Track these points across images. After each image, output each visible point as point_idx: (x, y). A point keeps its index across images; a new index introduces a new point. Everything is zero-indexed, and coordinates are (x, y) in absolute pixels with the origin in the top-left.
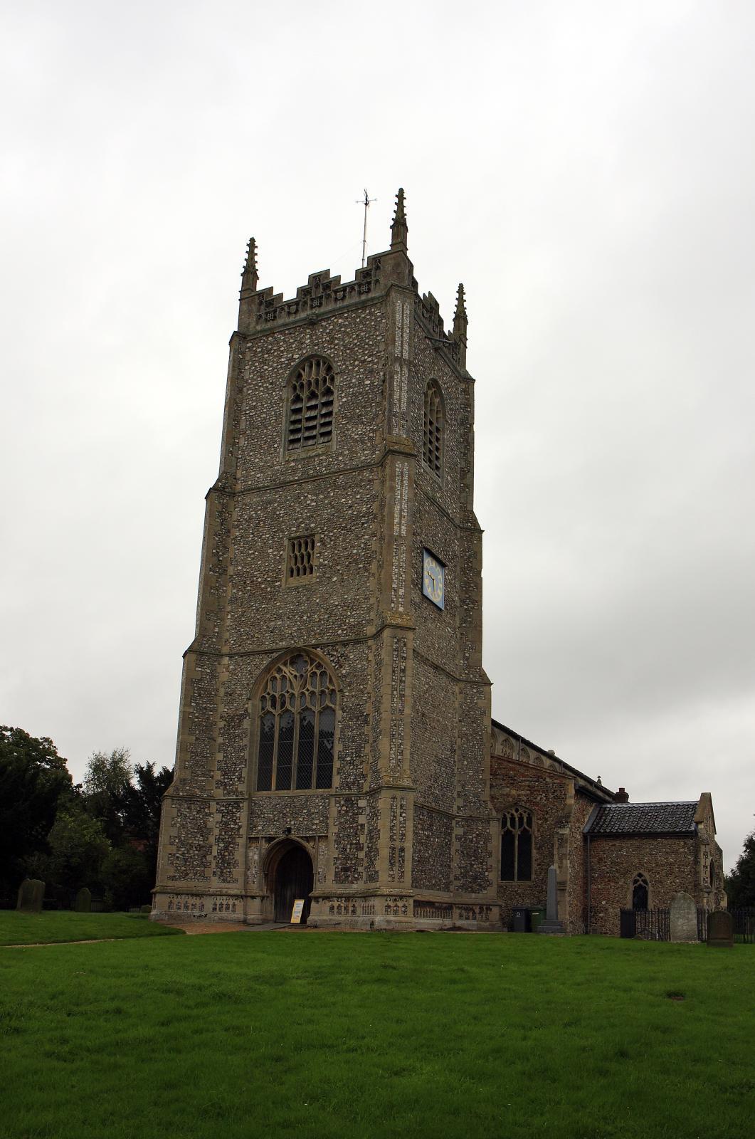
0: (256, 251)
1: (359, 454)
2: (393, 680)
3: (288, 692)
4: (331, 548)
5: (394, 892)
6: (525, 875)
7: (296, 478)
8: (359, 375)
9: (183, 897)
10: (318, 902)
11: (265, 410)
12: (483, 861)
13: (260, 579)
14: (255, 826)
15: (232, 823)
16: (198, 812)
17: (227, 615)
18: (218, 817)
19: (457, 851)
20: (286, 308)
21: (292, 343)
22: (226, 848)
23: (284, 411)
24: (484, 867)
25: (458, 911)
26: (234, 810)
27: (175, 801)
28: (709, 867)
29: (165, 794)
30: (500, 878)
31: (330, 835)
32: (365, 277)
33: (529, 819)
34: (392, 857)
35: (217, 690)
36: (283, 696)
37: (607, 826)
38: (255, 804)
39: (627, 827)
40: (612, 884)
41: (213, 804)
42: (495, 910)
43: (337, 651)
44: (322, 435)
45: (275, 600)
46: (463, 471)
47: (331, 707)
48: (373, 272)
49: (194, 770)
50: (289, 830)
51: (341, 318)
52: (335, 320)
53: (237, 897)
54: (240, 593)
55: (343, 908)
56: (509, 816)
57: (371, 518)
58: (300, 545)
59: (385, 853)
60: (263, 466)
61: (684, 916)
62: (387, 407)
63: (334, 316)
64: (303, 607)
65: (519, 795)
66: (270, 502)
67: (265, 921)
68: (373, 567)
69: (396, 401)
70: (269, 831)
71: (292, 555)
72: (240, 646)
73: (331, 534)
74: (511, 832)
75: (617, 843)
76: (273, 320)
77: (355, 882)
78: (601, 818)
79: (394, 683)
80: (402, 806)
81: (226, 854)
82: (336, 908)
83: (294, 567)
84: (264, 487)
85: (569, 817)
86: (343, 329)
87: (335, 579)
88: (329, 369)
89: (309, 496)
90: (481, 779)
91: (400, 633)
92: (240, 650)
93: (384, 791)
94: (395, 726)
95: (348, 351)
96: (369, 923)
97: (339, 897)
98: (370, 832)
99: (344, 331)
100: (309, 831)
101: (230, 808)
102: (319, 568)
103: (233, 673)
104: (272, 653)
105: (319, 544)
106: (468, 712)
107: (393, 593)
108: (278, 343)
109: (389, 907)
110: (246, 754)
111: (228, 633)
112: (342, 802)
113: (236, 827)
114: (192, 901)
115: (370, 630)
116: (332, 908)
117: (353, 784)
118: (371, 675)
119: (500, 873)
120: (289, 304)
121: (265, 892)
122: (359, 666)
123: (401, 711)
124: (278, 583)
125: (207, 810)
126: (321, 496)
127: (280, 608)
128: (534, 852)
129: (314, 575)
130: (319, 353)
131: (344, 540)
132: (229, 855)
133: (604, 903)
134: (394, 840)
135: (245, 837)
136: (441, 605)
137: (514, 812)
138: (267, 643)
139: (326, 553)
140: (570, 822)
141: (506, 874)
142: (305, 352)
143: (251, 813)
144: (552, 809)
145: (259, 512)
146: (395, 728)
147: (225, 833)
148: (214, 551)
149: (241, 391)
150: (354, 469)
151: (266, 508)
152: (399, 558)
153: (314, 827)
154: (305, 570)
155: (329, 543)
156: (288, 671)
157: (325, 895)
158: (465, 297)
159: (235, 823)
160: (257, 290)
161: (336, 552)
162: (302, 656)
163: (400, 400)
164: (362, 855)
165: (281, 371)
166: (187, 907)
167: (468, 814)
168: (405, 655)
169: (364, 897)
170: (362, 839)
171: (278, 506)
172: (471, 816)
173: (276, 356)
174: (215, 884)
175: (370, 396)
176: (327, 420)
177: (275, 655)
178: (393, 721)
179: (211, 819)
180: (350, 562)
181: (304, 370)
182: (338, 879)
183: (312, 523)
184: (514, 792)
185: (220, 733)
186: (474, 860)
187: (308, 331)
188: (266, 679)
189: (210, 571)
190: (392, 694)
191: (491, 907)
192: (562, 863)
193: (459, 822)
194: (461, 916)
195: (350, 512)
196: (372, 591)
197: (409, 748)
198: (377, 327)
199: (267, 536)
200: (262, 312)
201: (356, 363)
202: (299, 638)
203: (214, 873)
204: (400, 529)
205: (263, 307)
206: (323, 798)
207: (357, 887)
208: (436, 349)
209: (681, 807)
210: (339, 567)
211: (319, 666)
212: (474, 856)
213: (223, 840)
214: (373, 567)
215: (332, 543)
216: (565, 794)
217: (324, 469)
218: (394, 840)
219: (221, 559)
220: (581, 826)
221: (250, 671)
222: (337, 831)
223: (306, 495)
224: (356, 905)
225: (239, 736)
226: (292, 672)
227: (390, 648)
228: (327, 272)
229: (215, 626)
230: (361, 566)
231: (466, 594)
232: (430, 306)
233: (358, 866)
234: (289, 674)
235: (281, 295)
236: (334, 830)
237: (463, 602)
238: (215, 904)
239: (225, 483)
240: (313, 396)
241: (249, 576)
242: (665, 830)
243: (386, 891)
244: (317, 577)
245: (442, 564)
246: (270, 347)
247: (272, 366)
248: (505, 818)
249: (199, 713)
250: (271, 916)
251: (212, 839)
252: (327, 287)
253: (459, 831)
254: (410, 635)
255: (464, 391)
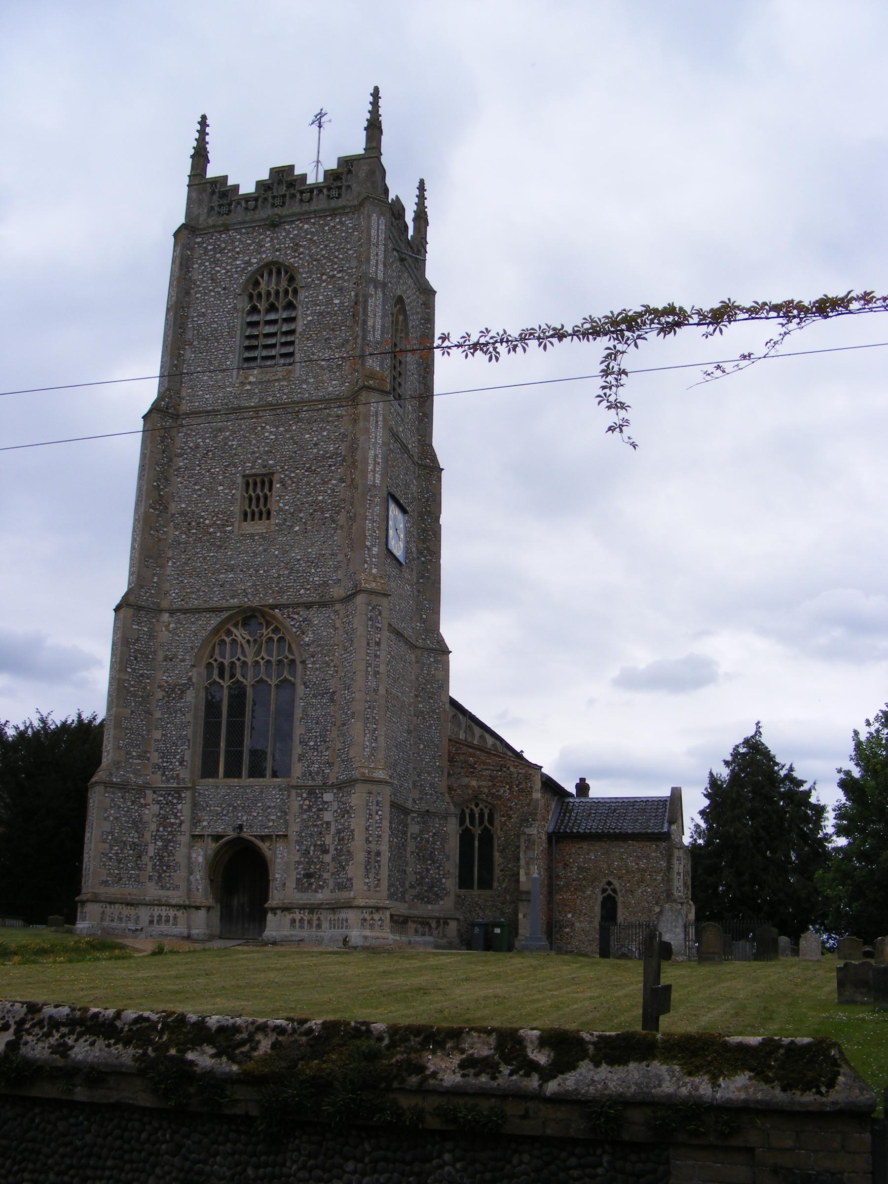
0: (208, 130)
1: (326, 384)
2: (368, 654)
3: (239, 659)
4: (292, 491)
5: (372, 902)
6: (486, 883)
7: (252, 404)
8: (327, 292)
9: (117, 906)
10: (275, 914)
11: (216, 320)
12: (440, 866)
13: (207, 522)
14: (199, 821)
15: (172, 817)
16: (133, 802)
17: (168, 561)
18: (155, 808)
19: (412, 852)
20: (243, 203)
21: (250, 245)
22: (165, 847)
23: (238, 322)
24: (441, 872)
25: (414, 926)
26: (175, 801)
27: (108, 789)
28: (682, 874)
29: (94, 780)
30: (457, 887)
31: (290, 833)
32: (334, 180)
33: (491, 816)
34: (368, 863)
35: (155, 653)
36: (233, 663)
37: (574, 825)
38: (200, 794)
39: (592, 825)
40: (580, 893)
41: (149, 792)
42: (453, 925)
43: (298, 614)
44: (283, 356)
45: (225, 549)
46: (422, 397)
47: (291, 680)
48: (344, 177)
49: (130, 751)
50: (241, 827)
51: (307, 224)
52: (300, 225)
53: (178, 907)
54: (184, 536)
55: (306, 922)
56: (467, 811)
57: (340, 461)
58: (255, 484)
59: (360, 857)
60: (213, 386)
61: (671, 930)
62: (360, 333)
63: (298, 220)
64: (259, 559)
65: (479, 787)
66: (220, 430)
67: (211, 938)
68: (341, 518)
69: (370, 329)
70: (216, 828)
71: (246, 495)
72: (182, 600)
73: (293, 475)
74: (470, 830)
75: (585, 845)
76: (227, 214)
77: (320, 891)
78: (565, 815)
79: (368, 658)
80: (378, 803)
81: (165, 854)
82: (297, 922)
83: (248, 510)
84: (214, 411)
85: (536, 814)
86: (309, 236)
87: (297, 528)
88: (292, 279)
89: (268, 427)
90: (439, 766)
91: (375, 600)
92: (183, 605)
93: (359, 785)
94: (369, 708)
95: (315, 263)
96: (341, 939)
97: (302, 908)
98: (339, 832)
99: (311, 239)
100: (265, 828)
101: (170, 798)
102: (278, 514)
103: (174, 632)
104: (221, 611)
105: (278, 485)
106: (425, 684)
107: (366, 552)
108: (233, 242)
109: (365, 920)
110: (188, 732)
111: (168, 584)
112: (305, 795)
113: (178, 821)
114: (126, 911)
115: (337, 592)
116: (293, 921)
117: (318, 773)
118: (338, 645)
119: (457, 879)
120: (247, 198)
121: (210, 902)
122: (325, 634)
123: (376, 691)
124: (230, 528)
125: (142, 801)
126: (282, 429)
127: (231, 558)
128: (497, 855)
129: (273, 521)
130: (281, 260)
131: (308, 484)
132: (169, 856)
133: (570, 916)
134: (370, 842)
135: (188, 834)
136: (402, 560)
137: (473, 807)
138: (216, 599)
139: (287, 497)
140: (537, 820)
141: (465, 882)
142: (264, 256)
143: (195, 805)
144: (516, 804)
145: (207, 441)
146: (369, 710)
147: (164, 828)
148: (155, 484)
149: (188, 293)
150: (321, 401)
151: (216, 436)
152: (373, 511)
153: (271, 824)
154: (261, 513)
155: (290, 486)
156: (240, 634)
157: (284, 906)
158: (426, 194)
159: (176, 817)
160: (208, 177)
161: (298, 496)
162: (256, 617)
163: (374, 327)
164: (327, 858)
165: (236, 276)
166: (120, 919)
167: (424, 807)
168: (380, 626)
169: (333, 909)
170: (328, 839)
171: (231, 435)
172: (428, 811)
173: (230, 257)
174: (153, 891)
175: (340, 318)
176: (289, 339)
177: (225, 615)
178: (367, 702)
179: (147, 812)
180: (315, 511)
181: (262, 277)
182: (301, 887)
183: (271, 459)
184: (474, 783)
185: (157, 706)
186: (430, 865)
187: (268, 233)
188: (212, 644)
189: (150, 508)
190: (367, 671)
191: (449, 921)
192: (529, 869)
193: (415, 817)
194: (416, 931)
195: (315, 451)
196: (339, 546)
197: (383, 734)
198: (348, 240)
199: (217, 470)
200: (215, 204)
201: (324, 277)
202: (254, 596)
203: (150, 878)
204: (374, 477)
205: (215, 197)
206: (280, 790)
207: (321, 896)
208: (402, 260)
209: (650, 804)
210: (301, 515)
211: (276, 630)
212: (430, 859)
213: (161, 837)
214: (341, 518)
215: (294, 485)
216: (531, 787)
217: (285, 397)
218: (370, 842)
219: (162, 493)
220: (546, 825)
221: (194, 631)
222: (298, 829)
223: (263, 425)
224: (322, 918)
225: (180, 710)
226: (245, 636)
227: (364, 617)
228: (291, 168)
229: (154, 575)
230: (328, 515)
231: (424, 543)
232: (397, 210)
233: (324, 871)
234: (240, 638)
235: (237, 187)
236: (294, 829)
237: (420, 553)
238: (152, 916)
239: (168, 403)
240: (272, 308)
241: (195, 516)
242: (636, 831)
243: (361, 902)
244: (276, 525)
245: (404, 511)
246: (223, 245)
247: (225, 269)
248: (463, 813)
249: (135, 681)
250: (217, 931)
251: (148, 836)
252: (291, 185)
253: (414, 829)
254: (384, 601)
255: (424, 304)
